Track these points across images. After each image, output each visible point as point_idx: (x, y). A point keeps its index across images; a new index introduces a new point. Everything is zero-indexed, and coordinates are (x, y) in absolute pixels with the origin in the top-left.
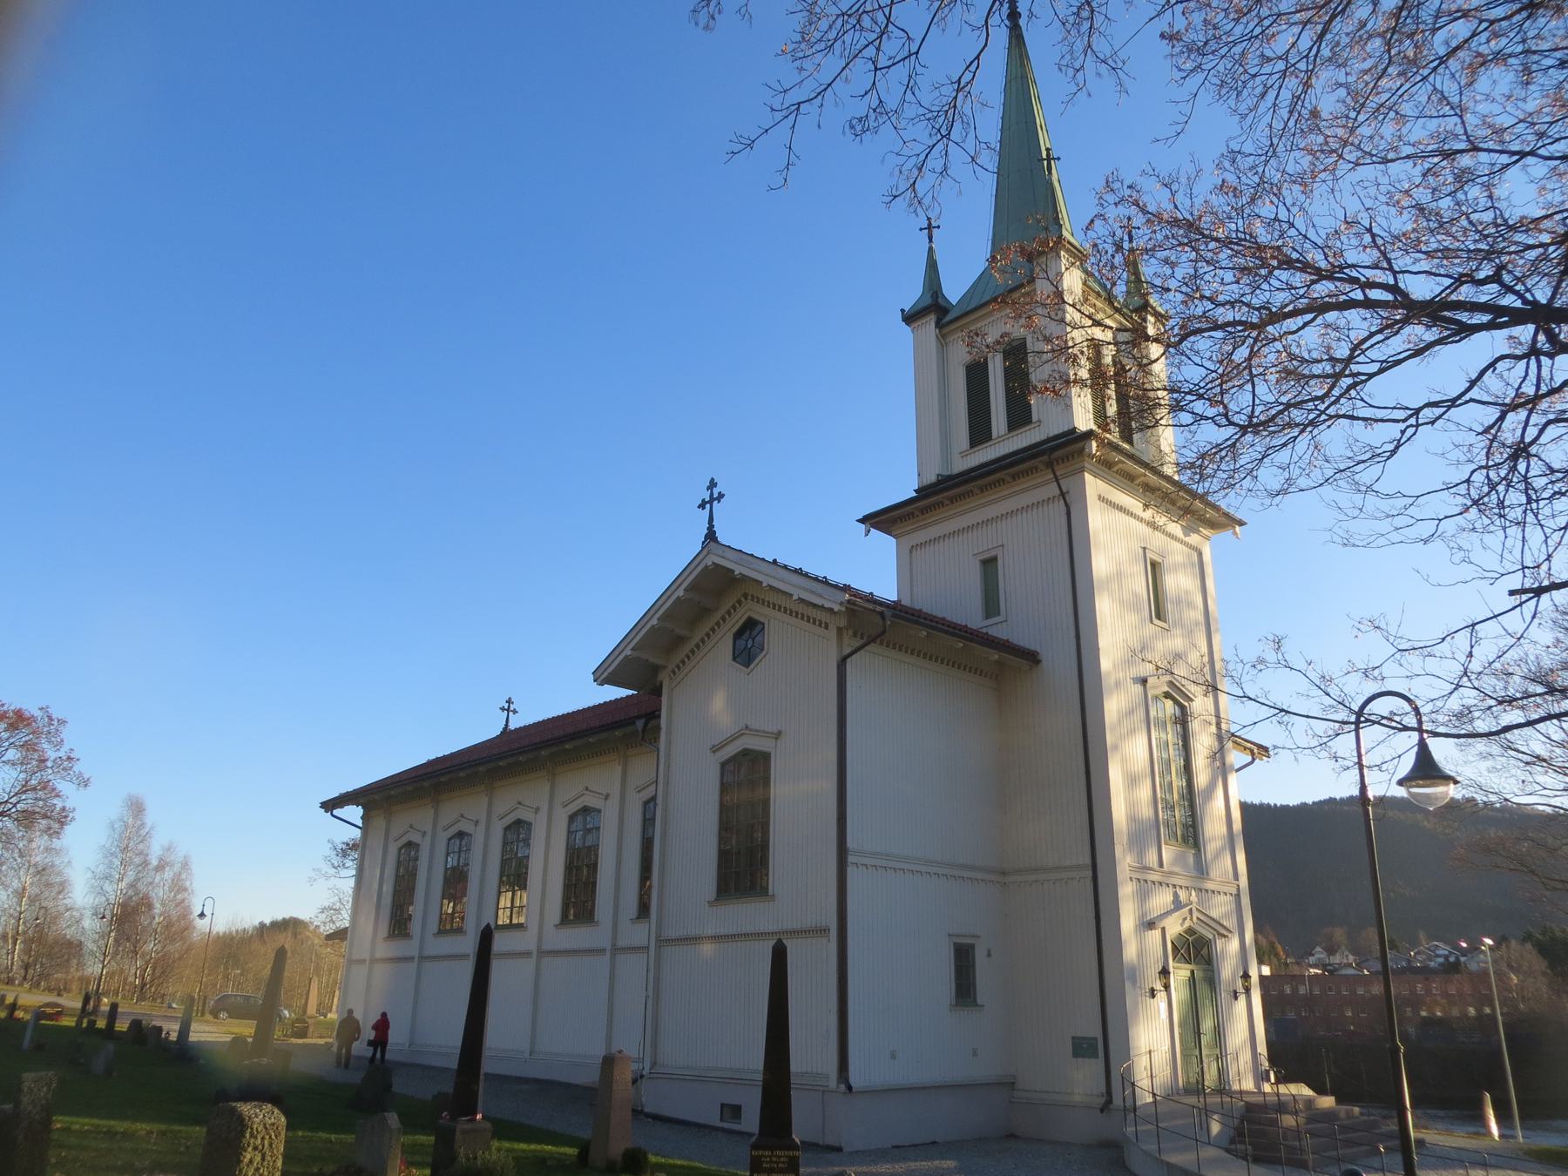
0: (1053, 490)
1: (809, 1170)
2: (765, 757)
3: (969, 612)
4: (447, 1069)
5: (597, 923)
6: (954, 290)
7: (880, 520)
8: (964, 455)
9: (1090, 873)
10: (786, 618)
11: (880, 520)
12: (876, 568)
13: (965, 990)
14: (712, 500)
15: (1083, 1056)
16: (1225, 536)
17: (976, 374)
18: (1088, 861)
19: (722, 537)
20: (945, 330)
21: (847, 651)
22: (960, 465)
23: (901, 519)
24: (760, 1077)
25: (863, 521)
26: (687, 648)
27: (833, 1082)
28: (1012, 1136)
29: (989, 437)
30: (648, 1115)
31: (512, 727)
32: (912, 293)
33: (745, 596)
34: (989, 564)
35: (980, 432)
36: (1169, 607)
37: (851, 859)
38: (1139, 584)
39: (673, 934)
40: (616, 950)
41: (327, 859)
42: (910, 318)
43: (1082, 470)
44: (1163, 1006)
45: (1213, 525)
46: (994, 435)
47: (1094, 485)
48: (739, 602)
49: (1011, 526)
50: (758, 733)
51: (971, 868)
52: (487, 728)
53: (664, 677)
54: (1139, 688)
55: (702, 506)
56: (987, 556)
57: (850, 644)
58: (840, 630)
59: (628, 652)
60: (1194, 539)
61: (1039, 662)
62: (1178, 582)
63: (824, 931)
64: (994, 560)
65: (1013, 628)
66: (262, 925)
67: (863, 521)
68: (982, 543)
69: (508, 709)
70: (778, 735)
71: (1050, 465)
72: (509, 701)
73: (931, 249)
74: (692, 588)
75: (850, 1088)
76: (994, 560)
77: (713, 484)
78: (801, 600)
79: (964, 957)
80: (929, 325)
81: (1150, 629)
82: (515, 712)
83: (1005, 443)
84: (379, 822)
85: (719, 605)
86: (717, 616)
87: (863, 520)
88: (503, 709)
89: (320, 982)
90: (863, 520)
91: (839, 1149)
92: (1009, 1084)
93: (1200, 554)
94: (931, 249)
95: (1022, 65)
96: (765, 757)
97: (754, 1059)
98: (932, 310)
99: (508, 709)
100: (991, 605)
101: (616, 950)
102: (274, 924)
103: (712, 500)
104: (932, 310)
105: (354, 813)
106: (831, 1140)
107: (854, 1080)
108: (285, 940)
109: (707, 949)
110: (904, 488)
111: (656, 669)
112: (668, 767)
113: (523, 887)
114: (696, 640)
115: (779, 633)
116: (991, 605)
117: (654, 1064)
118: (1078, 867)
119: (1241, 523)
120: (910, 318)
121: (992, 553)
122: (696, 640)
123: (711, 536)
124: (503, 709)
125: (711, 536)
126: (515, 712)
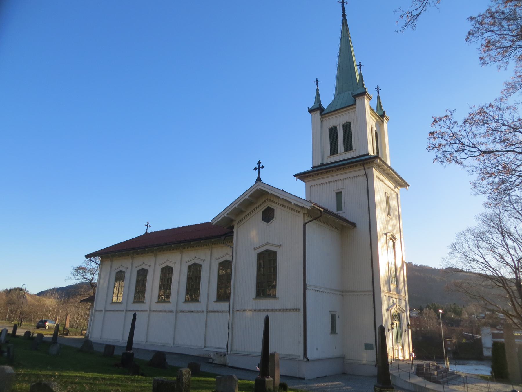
0: (363, 172)
1: (249, 382)
2: (275, 253)
3: (332, 207)
4: (123, 347)
5: (200, 302)
6: (325, 104)
7: (301, 176)
8: (328, 157)
9: (372, 293)
10: (281, 207)
11: (301, 176)
12: (299, 190)
13: (333, 330)
14: (259, 168)
15: (368, 349)
16: (404, 189)
17: (333, 131)
18: (372, 290)
19: (263, 180)
20: (323, 116)
21: (306, 221)
22: (327, 161)
23: (308, 176)
24: (260, 354)
25: (295, 176)
26: (244, 215)
27: (302, 358)
28: (344, 374)
29: (337, 153)
30: (230, 367)
31: (149, 231)
32: (311, 103)
33: (267, 199)
34: (339, 194)
35: (334, 151)
36: (391, 211)
37: (307, 287)
38: (384, 204)
39: (239, 308)
40: (208, 311)
41: (72, 273)
42: (311, 111)
43: (372, 167)
44: (391, 334)
45: (401, 186)
46: (339, 152)
47: (376, 173)
48: (265, 201)
49: (348, 182)
50: (272, 245)
51: (334, 290)
52: (139, 232)
53: (235, 224)
54: (385, 236)
55: (256, 169)
56: (338, 191)
57: (307, 219)
58: (304, 214)
59: (225, 215)
60: (396, 190)
61: (356, 226)
62: (393, 203)
63: (299, 310)
64: (341, 192)
65: (348, 213)
66: (6, 290)
67: (295, 176)
68: (337, 186)
69: (147, 225)
70: (280, 246)
71: (363, 165)
72: (148, 223)
73: (317, 89)
74: (250, 196)
75: (308, 360)
76: (341, 192)
77: (259, 162)
78: (295, 204)
79: (333, 317)
80: (317, 114)
81: (388, 218)
82: (150, 226)
83: (342, 156)
84: (108, 264)
85: (261, 202)
86: (257, 205)
87: (296, 176)
88: (146, 225)
89: (71, 316)
90: (296, 176)
91: (304, 379)
92: (343, 357)
93: (397, 195)
94: (317, 89)
95: (347, 32)
96: (275, 253)
97: (259, 349)
98: (317, 109)
99: (147, 225)
100: (339, 206)
101: (208, 311)
102: (11, 290)
103: (259, 168)
104: (317, 109)
105: (98, 259)
106: (301, 376)
107: (309, 356)
108: (15, 296)
109: (249, 314)
110: (308, 167)
111: (232, 221)
112: (236, 253)
113: (123, 281)
114: (248, 212)
115: (279, 212)
116: (339, 206)
117: (231, 350)
118: (368, 291)
119: (409, 186)
120: (311, 111)
121: (340, 191)
122: (248, 212)
123: (259, 179)
124: (146, 225)
125: (259, 179)
126: (150, 226)
